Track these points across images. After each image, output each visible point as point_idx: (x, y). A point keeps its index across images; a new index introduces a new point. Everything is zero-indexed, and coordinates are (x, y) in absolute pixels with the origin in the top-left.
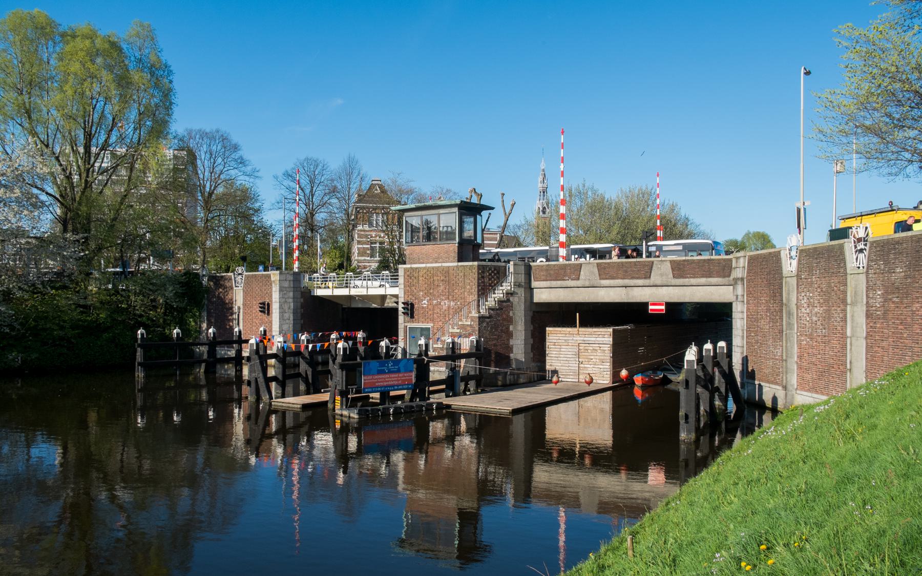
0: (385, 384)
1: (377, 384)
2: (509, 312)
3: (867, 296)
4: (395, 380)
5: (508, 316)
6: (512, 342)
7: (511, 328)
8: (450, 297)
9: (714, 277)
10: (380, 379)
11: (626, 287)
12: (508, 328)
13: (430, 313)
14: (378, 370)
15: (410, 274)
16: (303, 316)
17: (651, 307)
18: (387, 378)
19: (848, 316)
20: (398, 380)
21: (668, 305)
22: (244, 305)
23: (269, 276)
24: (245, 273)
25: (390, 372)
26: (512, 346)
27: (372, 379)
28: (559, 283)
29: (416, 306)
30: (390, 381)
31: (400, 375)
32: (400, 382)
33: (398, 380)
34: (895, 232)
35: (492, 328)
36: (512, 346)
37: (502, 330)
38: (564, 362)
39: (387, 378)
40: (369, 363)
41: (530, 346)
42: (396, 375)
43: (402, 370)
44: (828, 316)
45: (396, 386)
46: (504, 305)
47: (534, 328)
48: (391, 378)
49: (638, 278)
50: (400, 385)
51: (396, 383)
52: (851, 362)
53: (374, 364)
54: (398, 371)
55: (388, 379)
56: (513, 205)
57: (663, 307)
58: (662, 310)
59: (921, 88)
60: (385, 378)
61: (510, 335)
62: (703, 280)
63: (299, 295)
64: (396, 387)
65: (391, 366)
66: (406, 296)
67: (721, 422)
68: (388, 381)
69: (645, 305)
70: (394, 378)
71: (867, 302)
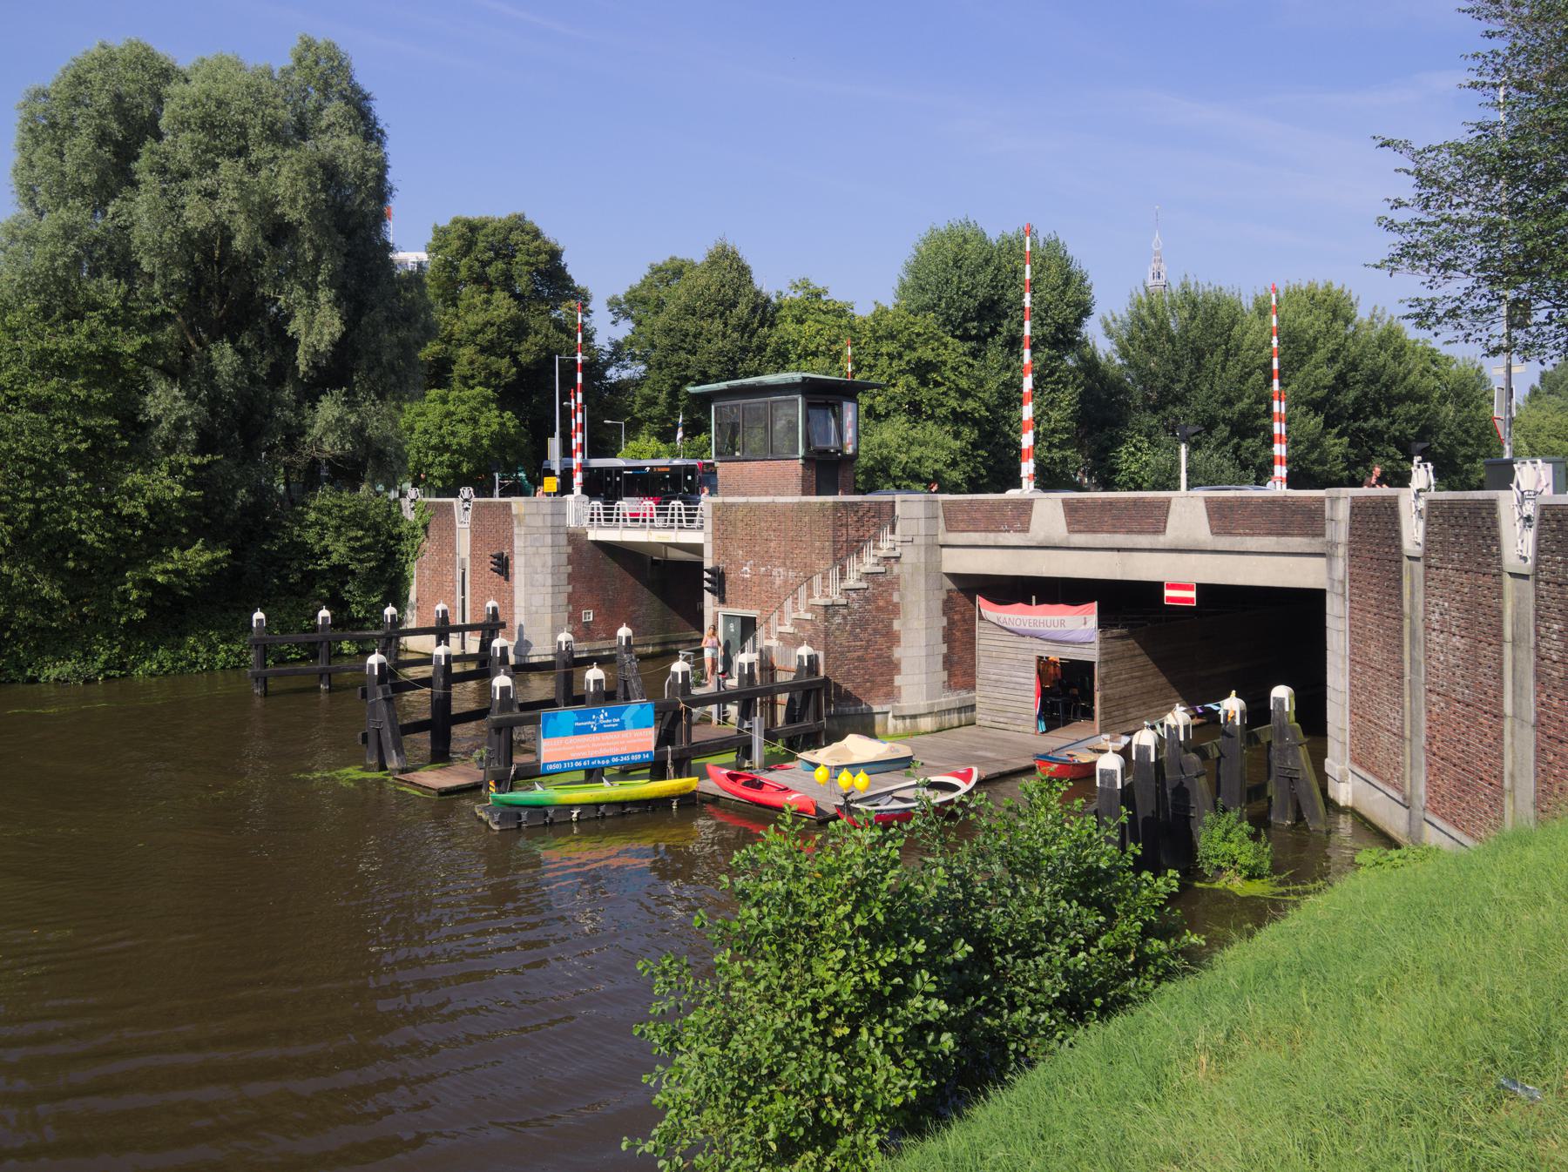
2: (891, 595)
3: (1537, 633)
5: (889, 602)
6: (898, 653)
7: (896, 625)
8: (788, 563)
9: (1292, 535)
10: (580, 744)
11: (1119, 550)
12: (890, 625)
13: (755, 589)
15: (721, 513)
16: (571, 578)
17: (1168, 593)
19: (1508, 667)
21: (1203, 589)
22: (473, 556)
23: (508, 505)
24: (474, 499)
26: (899, 660)
27: (563, 745)
28: (991, 538)
29: (731, 577)
35: (854, 626)
36: (899, 660)
37: (874, 630)
38: (1009, 691)
40: (555, 716)
41: (940, 659)
43: (628, 723)
44: (1472, 660)
46: (881, 584)
47: (949, 623)
49: (1141, 532)
52: (1512, 776)
53: (566, 715)
54: (621, 727)
57: (1192, 594)
58: (1191, 600)
59: (1566, 168)
61: (892, 638)
62: (1270, 543)
63: (563, 540)
65: (605, 718)
66: (716, 557)
68: (598, 748)
69: (1156, 588)
70: (611, 741)
71: (1537, 645)
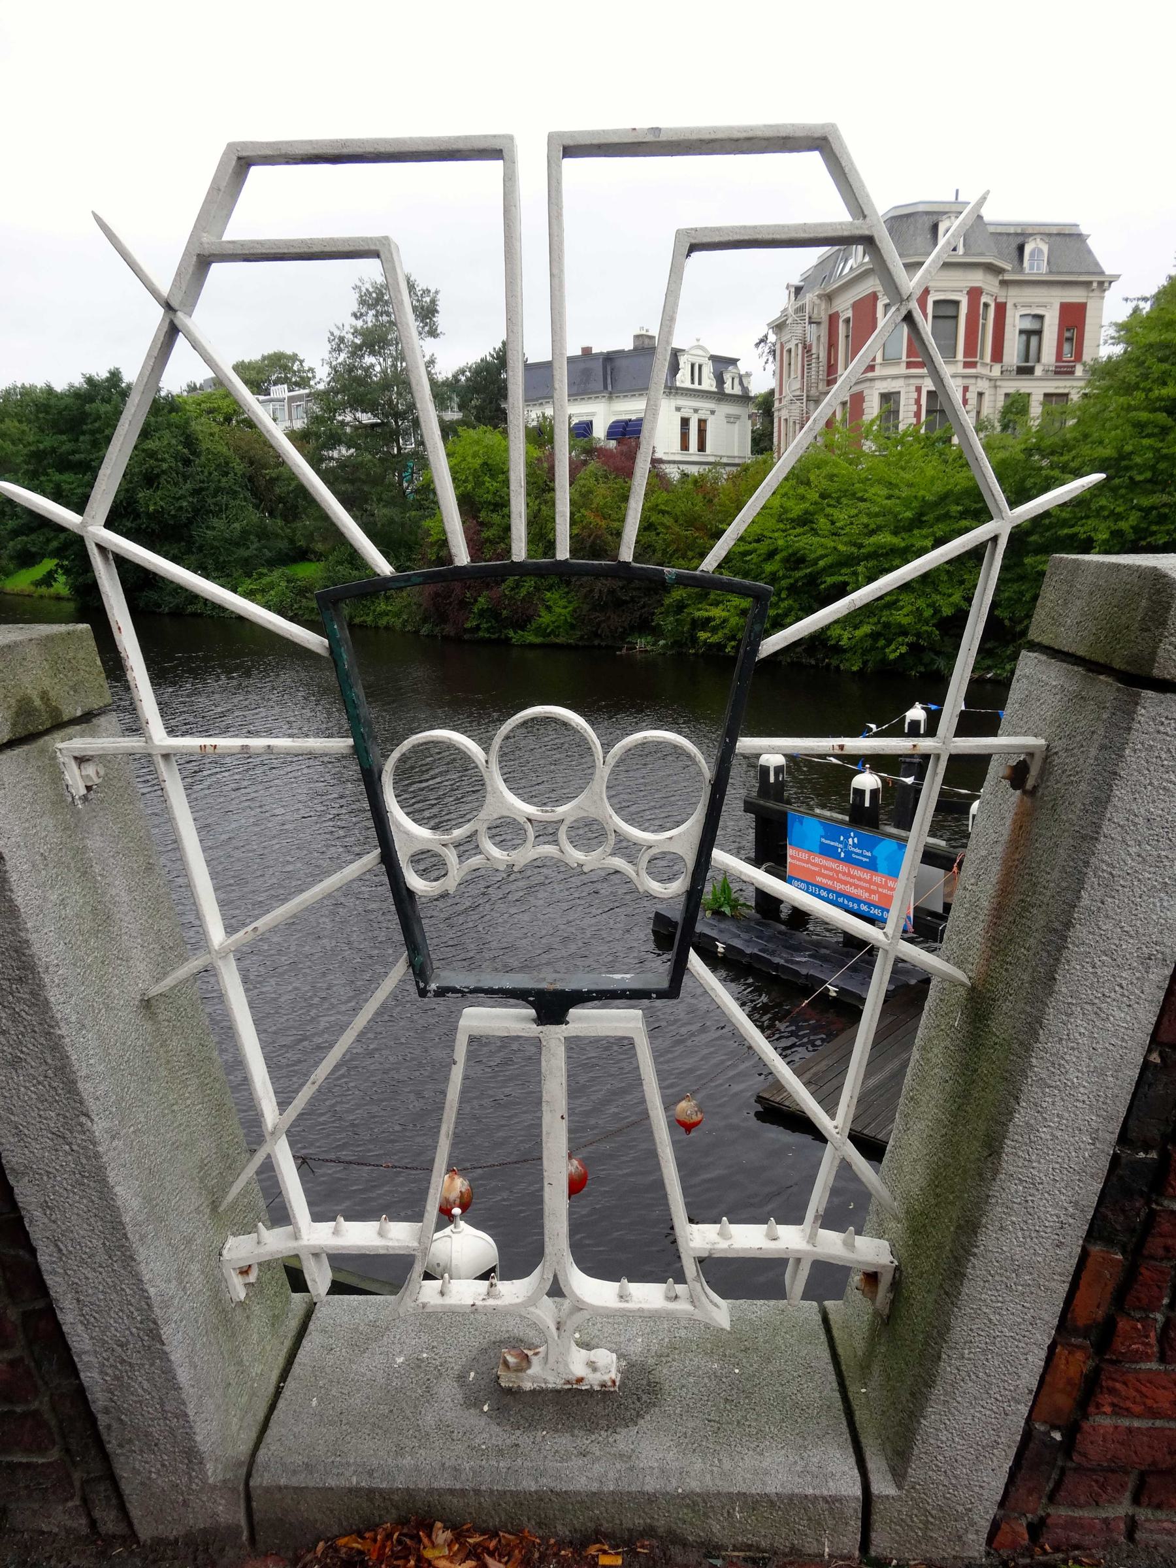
0: (839, 887)
1: (819, 879)
4: (862, 888)
14: (822, 845)
18: (844, 874)
20: (871, 892)
25: (849, 860)
27: (808, 862)
30: (852, 885)
31: (877, 879)
32: (875, 898)
33: (871, 892)
34: (701, 1261)
39: (844, 874)
42: (867, 876)
45: (825, 889)
48: (853, 877)
50: (876, 907)
51: (865, 895)
55: (844, 878)
56: (1126, 300)
60: (838, 872)
64: (824, 894)
65: (854, 845)
67: (942, 636)
